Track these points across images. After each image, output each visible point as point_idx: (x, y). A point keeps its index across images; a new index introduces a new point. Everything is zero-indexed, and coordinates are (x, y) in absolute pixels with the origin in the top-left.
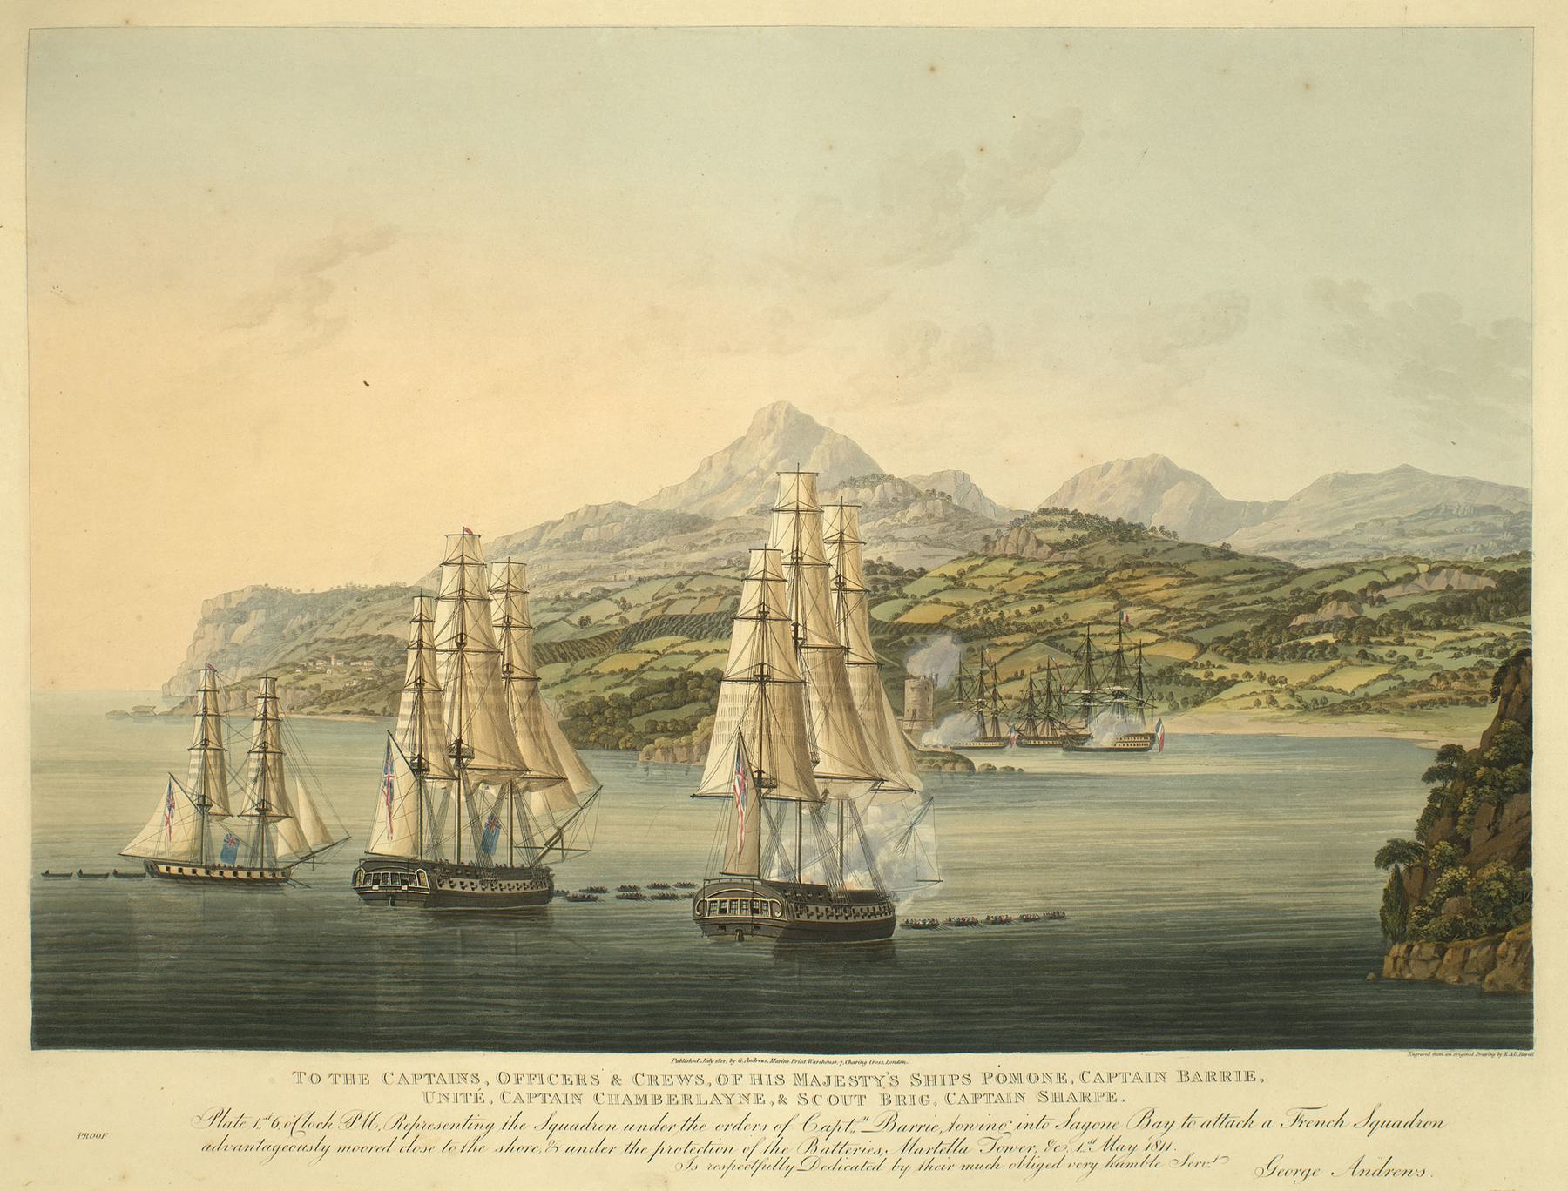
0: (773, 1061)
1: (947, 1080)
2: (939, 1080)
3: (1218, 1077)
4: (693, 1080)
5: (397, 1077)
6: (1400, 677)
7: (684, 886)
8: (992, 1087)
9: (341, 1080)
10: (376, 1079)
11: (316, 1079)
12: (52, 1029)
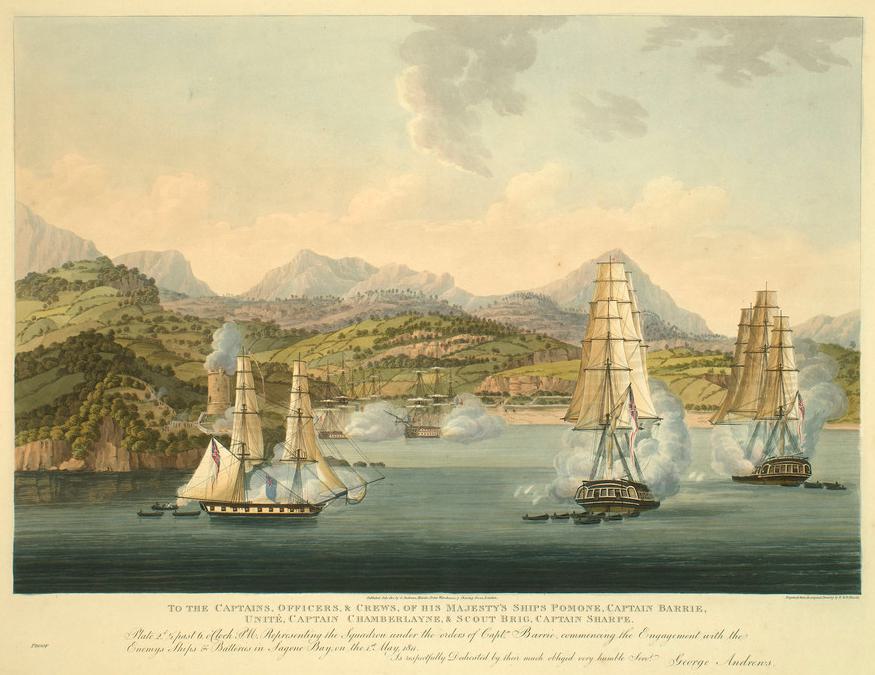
0: (419, 598)
3: (682, 609)
7: (637, 465)
8: (558, 612)
9: (193, 609)
10: (211, 608)
11: (179, 609)
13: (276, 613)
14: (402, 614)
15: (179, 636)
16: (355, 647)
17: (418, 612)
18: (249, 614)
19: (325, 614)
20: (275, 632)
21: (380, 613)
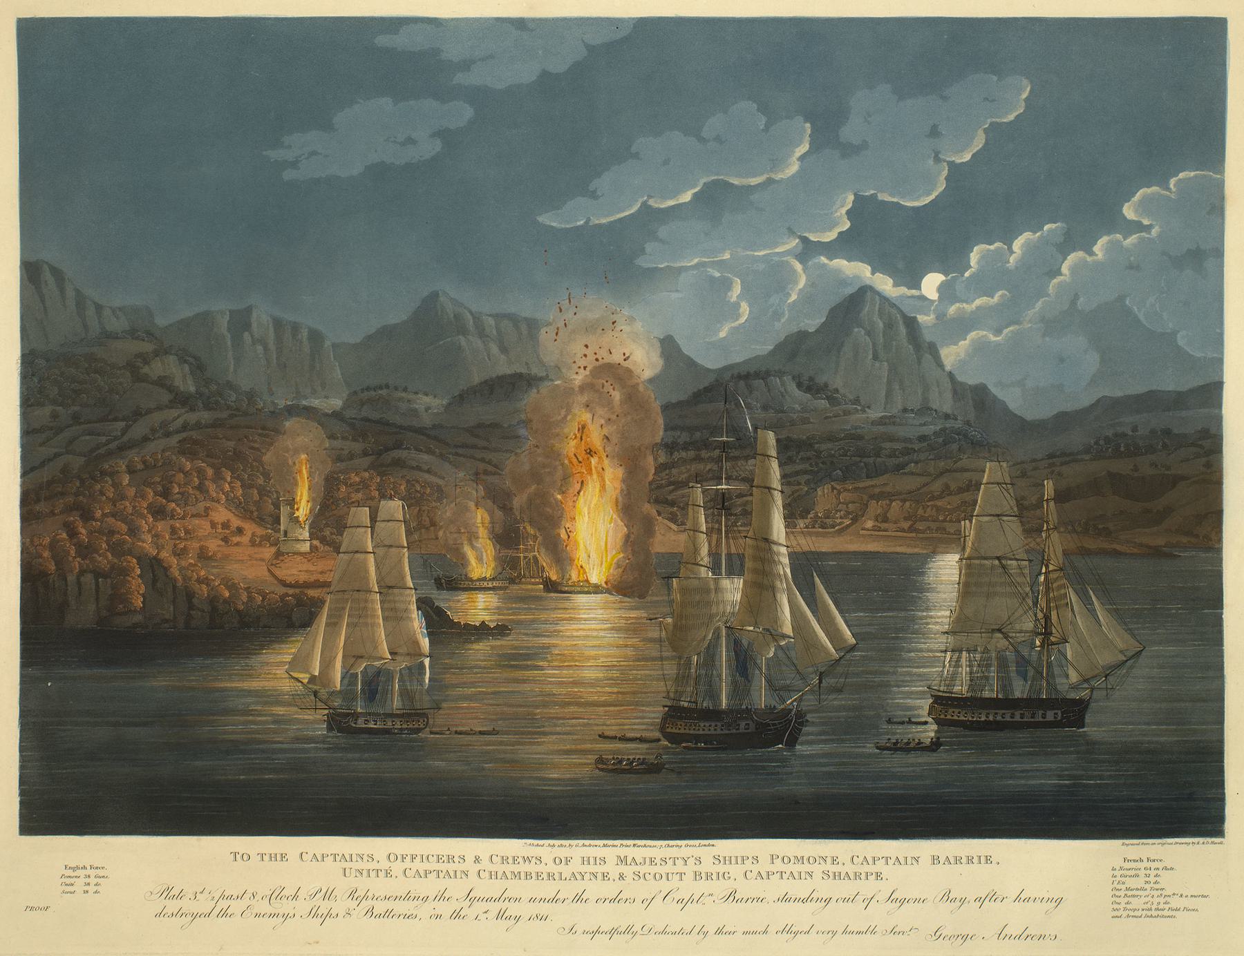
0: (687, 846)
1: (983, 859)
2: (592, 861)
4: (534, 860)
5: (310, 856)
6: (1201, 446)
9: (266, 858)
12: (55, 805)
13: (385, 864)
14: (552, 868)
15: (222, 896)
16: (224, 914)
17: (576, 866)
18: (347, 865)
19: (451, 867)
20: (361, 893)
21: (523, 868)
